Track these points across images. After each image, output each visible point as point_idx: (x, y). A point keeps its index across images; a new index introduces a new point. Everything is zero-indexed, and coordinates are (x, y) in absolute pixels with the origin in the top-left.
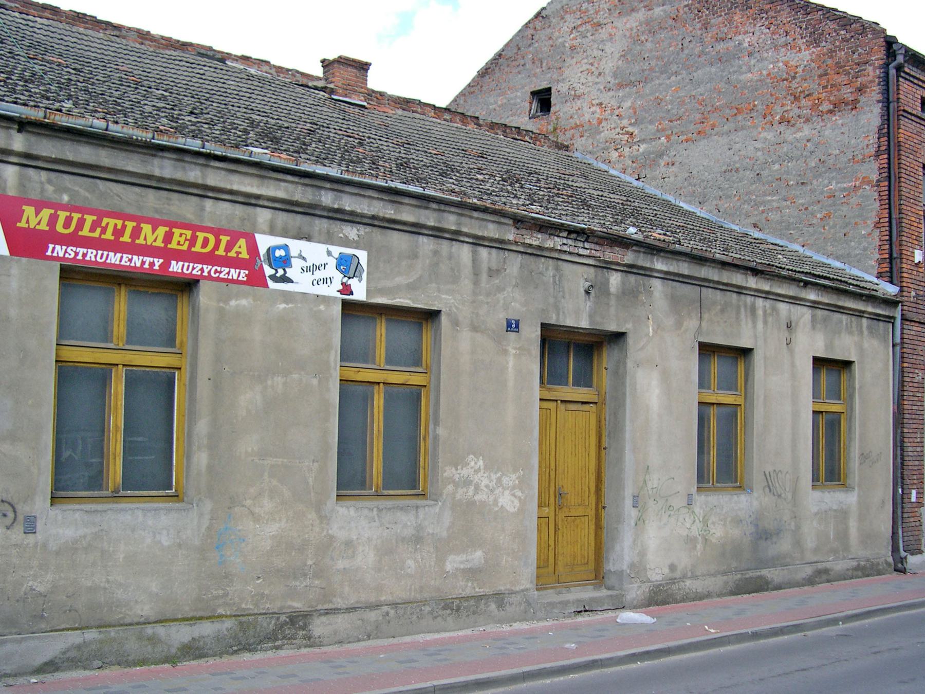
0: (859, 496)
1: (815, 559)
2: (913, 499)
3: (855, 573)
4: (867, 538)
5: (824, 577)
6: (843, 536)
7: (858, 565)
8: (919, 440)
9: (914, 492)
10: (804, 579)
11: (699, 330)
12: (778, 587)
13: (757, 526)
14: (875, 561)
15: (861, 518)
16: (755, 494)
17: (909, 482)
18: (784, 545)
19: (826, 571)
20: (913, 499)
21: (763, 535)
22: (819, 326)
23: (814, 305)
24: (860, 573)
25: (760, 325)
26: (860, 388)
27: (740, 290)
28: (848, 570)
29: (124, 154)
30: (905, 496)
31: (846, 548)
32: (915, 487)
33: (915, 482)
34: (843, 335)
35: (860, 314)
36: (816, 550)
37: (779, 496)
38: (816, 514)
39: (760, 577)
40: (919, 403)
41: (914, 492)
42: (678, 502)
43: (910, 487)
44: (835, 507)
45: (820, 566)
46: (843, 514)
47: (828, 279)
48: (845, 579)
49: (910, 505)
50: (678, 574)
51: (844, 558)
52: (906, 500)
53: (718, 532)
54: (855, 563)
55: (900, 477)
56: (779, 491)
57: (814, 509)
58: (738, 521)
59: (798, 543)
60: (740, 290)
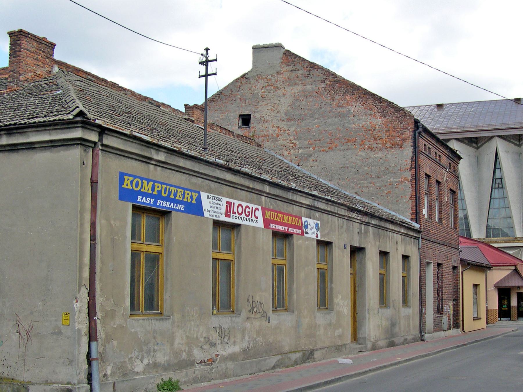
16: (391, 309)
18: (397, 330)
42: (376, 312)
57: (403, 315)
59: (400, 328)
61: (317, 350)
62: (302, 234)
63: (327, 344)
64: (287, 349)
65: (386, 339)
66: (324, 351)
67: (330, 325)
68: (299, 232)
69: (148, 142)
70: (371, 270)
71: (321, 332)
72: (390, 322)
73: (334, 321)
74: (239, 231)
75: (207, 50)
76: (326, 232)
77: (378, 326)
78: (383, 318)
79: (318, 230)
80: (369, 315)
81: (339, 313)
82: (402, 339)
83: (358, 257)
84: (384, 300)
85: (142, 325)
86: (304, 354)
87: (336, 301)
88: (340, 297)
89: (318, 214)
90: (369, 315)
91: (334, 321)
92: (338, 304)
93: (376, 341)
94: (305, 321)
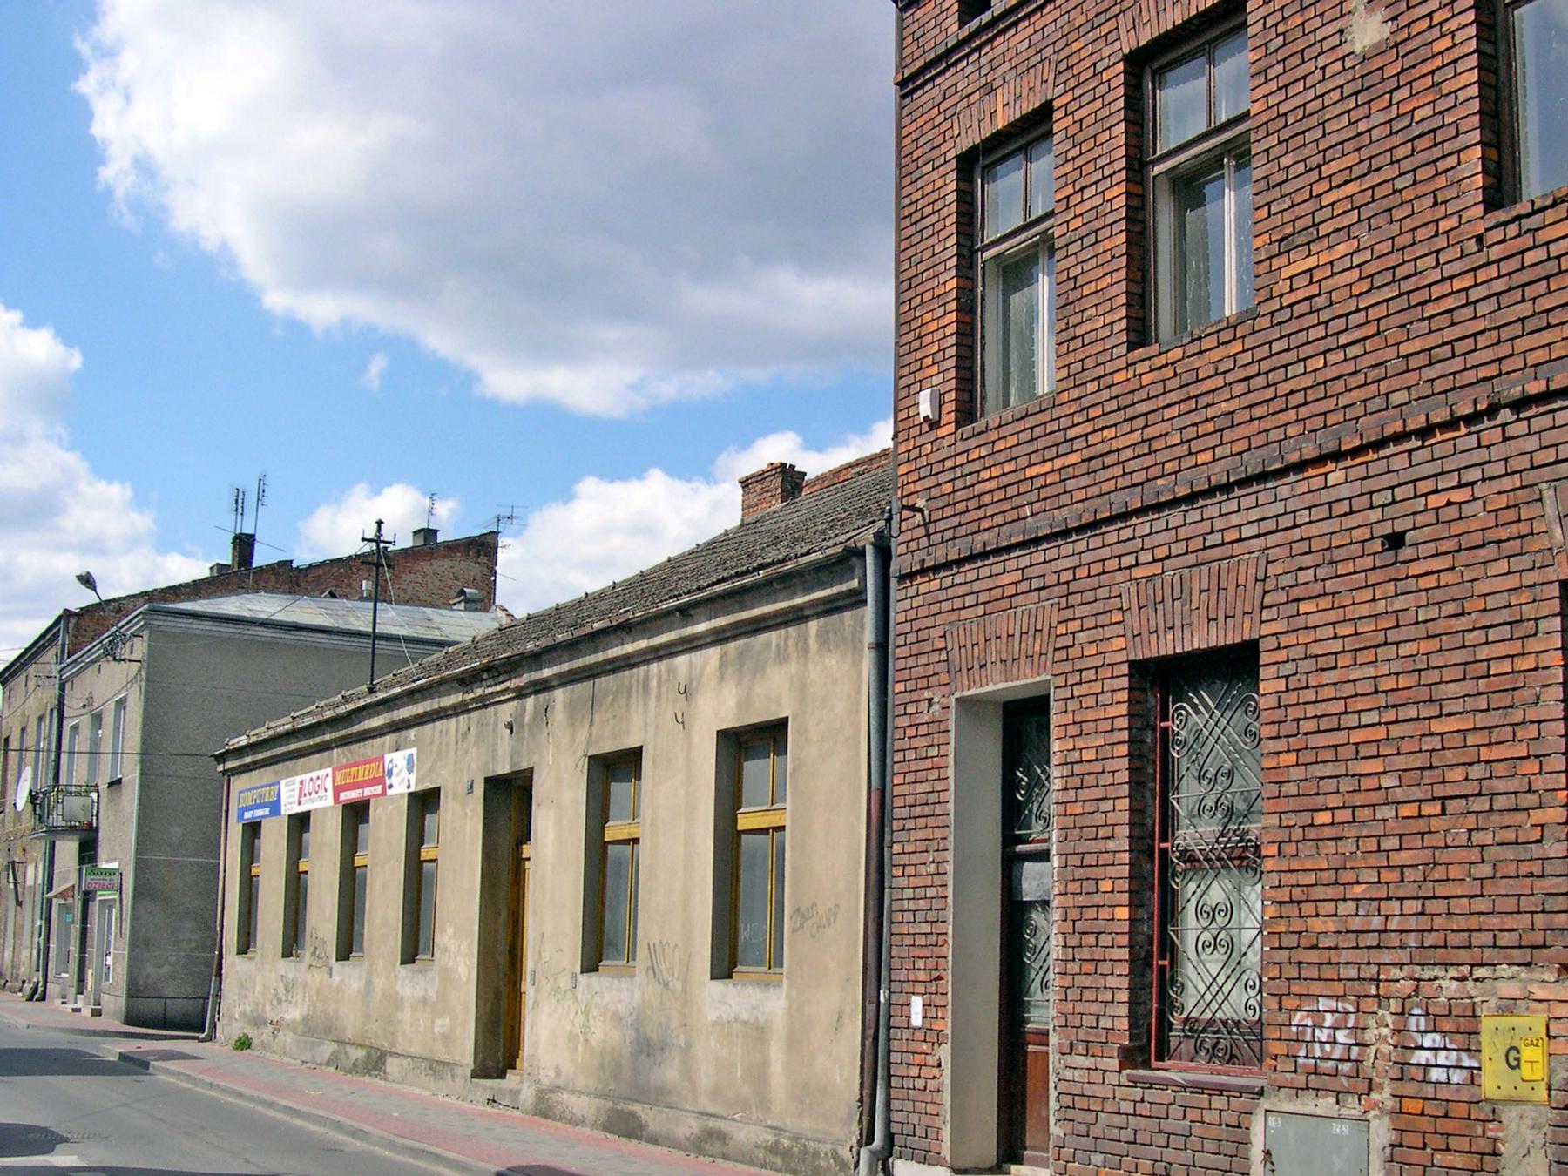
0: (788, 997)
1: (711, 1110)
2: (917, 1021)
3: (771, 1158)
4: (806, 1093)
5: (718, 1147)
6: (759, 1076)
7: (777, 1143)
8: (932, 869)
9: (917, 1003)
10: (687, 1139)
11: (588, 744)
12: (653, 1140)
13: (637, 1030)
14: (811, 1146)
15: (794, 1042)
16: (637, 979)
17: (903, 975)
18: (669, 1073)
19: (721, 1136)
20: (917, 1021)
21: (647, 1048)
22: (730, 671)
23: (720, 637)
24: (779, 1161)
25: (652, 703)
26: (795, 770)
27: (627, 663)
28: (757, 1146)
29: (1020, 696)
30: (895, 1010)
31: (764, 1103)
32: (920, 988)
33: (922, 976)
34: (769, 671)
35: (797, 617)
36: (716, 1093)
37: (666, 985)
38: (714, 1024)
39: (632, 1115)
40: (934, 775)
41: (917, 1003)
42: (564, 982)
43: (907, 987)
44: (745, 1016)
45: (712, 1124)
46: (757, 1033)
47: (724, 580)
48: (752, 1163)
49: (907, 1034)
50: (561, 1083)
51: (758, 1123)
52: (894, 1021)
53: (600, 1032)
54: (770, 1138)
55: (877, 967)
56: (666, 976)
57: (712, 1016)
58: (617, 1019)
59: (688, 1072)
60: (627, 663)
61: (398, 1055)
62: (384, 793)
63: (415, 1049)
64: (349, 1035)
65: (603, 1096)
66: (405, 1062)
67: (424, 1000)
68: (379, 789)
69: (312, 726)
70: (551, 836)
71: (406, 1015)
72: (631, 1034)
73: (432, 994)
74: (780, 748)
75: (380, 523)
76: (428, 765)
77: (572, 1037)
78: (595, 1012)
79: (410, 771)
80: (537, 992)
81: (447, 976)
82: (689, 1126)
83: (756, 770)
84: (601, 944)
85: (240, 959)
86: (369, 1055)
87: (440, 940)
88: (450, 931)
89: (412, 733)
90: (537, 992)
91: (432, 994)
92: (445, 950)
93: (556, 1089)
94: (379, 983)
